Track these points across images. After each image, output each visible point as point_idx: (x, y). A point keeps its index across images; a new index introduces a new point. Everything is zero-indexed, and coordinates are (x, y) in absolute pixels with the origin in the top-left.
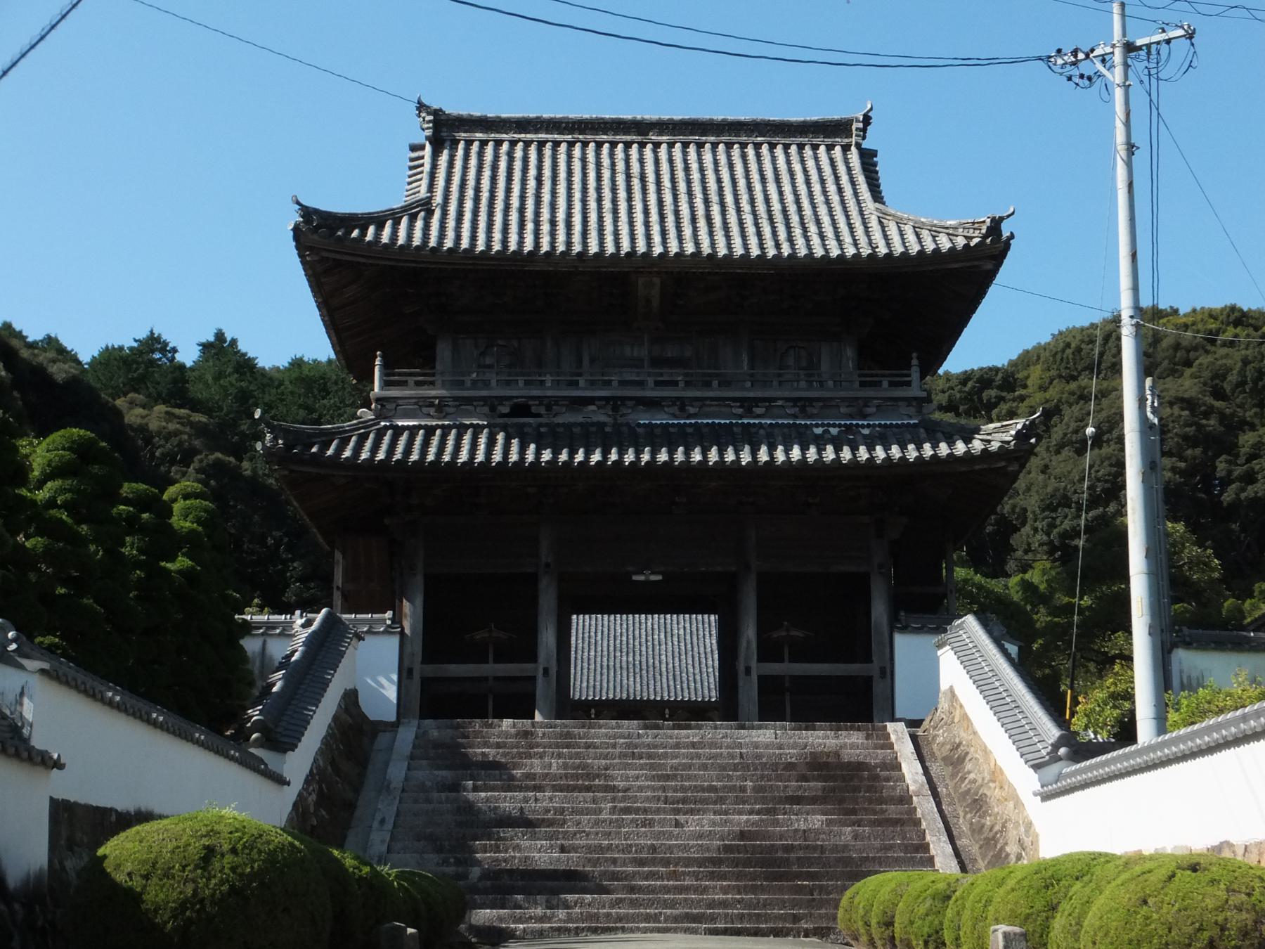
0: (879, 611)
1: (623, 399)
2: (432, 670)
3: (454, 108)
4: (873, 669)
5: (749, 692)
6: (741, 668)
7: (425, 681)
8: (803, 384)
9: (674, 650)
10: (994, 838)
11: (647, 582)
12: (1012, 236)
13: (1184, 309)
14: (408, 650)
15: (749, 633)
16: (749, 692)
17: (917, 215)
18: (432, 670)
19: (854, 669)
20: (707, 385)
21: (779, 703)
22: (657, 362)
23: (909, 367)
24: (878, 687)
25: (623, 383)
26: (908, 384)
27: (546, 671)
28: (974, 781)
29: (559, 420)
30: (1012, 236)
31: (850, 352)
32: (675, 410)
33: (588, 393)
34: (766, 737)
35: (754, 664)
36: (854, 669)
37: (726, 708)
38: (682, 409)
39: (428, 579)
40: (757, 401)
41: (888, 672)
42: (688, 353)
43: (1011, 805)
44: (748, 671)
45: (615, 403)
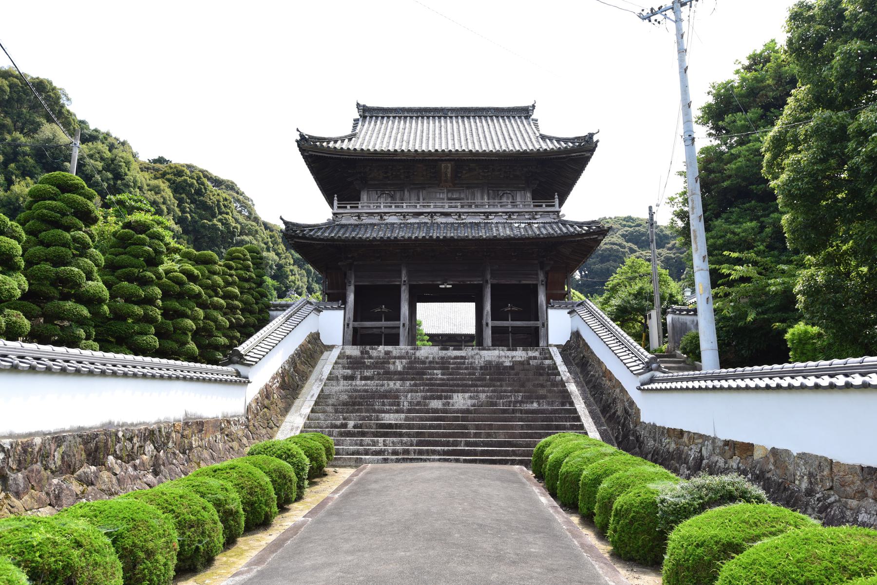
0: (542, 298)
1: (435, 213)
2: (357, 324)
3: (370, 104)
4: (539, 324)
5: (488, 333)
6: (484, 323)
7: (355, 330)
8: (510, 206)
9: (454, 317)
10: (609, 406)
11: (446, 288)
12: (597, 141)
13: (780, 35)
14: (347, 317)
15: (488, 307)
16: (488, 333)
17: (557, 124)
18: (357, 324)
19: (531, 323)
20: (470, 206)
21: (501, 339)
22: (449, 199)
23: (554, 198)
24: (542, 332)
25: (435, 207)
26: (553, 206)
27: (404, 325)
28: (593, 376)
29: (409, 221)
30: (597, 141)
31: (529, 195)
32: (456, 217)
33: (421, 211)
34: (492, 355)
35: (490, 321)
36: (531, 323)
37: (476, 340)
38: (460, 216)
39: (356, 286)
40: (491, 213)
41: (545, 325)
42: (462, 196)
43: (618, 390)
44: (487, 324)
45: (432, 214)
